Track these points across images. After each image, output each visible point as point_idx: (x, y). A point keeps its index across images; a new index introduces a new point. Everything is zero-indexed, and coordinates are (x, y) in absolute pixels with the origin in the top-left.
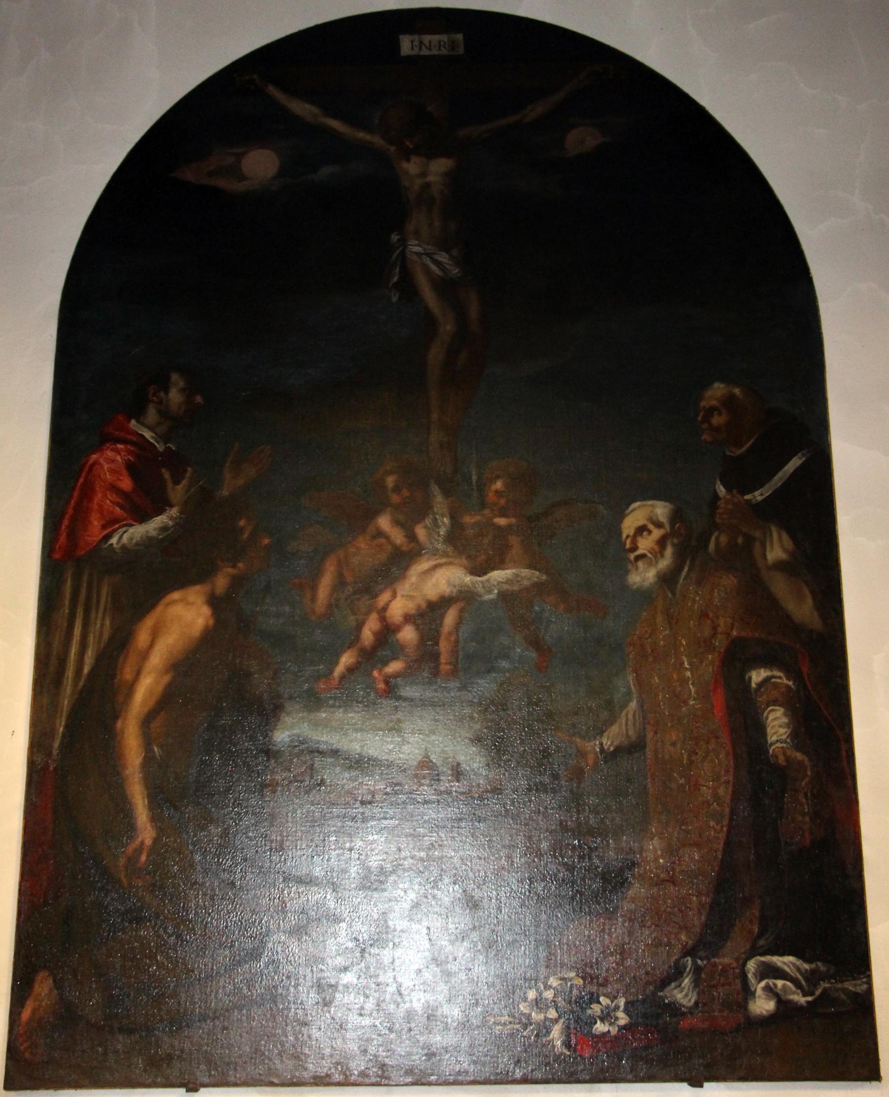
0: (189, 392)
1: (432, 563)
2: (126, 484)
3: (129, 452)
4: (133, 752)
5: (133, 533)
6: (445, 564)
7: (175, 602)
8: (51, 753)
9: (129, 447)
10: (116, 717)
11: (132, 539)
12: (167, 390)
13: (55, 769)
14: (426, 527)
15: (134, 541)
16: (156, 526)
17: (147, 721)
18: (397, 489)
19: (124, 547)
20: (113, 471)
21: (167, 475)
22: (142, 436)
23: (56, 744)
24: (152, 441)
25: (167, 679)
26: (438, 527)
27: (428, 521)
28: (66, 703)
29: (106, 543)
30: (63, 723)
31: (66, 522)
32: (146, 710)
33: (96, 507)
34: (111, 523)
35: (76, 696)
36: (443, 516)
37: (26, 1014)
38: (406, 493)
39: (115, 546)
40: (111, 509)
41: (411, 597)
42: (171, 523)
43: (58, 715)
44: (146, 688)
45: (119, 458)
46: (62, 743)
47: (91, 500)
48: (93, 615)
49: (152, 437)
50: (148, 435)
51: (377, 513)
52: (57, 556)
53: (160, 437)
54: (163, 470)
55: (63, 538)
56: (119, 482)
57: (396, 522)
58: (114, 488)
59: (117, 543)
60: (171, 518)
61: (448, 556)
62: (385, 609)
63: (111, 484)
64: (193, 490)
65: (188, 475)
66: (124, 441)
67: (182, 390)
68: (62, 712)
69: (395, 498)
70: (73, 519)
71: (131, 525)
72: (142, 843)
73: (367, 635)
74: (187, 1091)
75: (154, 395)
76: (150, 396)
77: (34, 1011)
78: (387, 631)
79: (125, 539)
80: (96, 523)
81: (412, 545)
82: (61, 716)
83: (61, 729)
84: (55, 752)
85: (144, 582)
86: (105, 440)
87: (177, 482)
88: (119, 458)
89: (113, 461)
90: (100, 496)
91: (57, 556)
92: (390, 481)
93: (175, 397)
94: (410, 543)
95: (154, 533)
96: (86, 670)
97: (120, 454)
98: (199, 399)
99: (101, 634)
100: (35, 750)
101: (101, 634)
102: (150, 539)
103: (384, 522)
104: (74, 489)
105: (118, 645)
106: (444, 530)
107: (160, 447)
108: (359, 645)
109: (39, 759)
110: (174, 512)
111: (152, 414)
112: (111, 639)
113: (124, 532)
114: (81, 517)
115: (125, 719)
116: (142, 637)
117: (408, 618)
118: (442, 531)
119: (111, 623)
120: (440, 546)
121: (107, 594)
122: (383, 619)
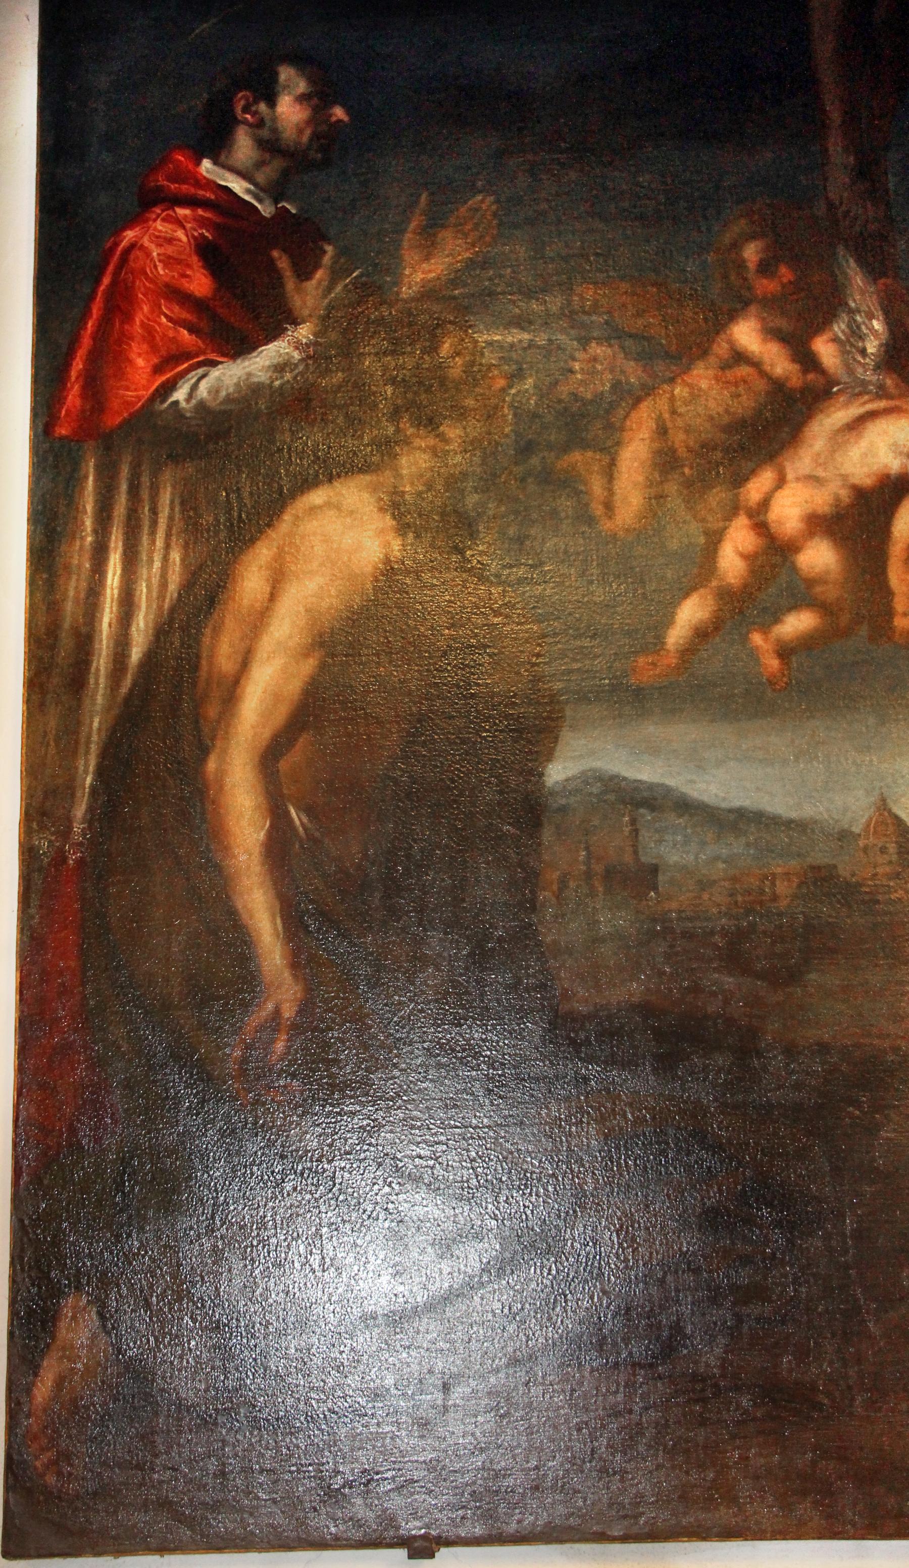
0: (319, 98)
1: (855, 411)
2: (200, 283)
3: (202, 222)
4: (244, 823)
5: (219, 379)
6: (887, 412)
7: (313, 510)
8: (66, 834)
9: (200, 212)
10: (204, 751)
11: (217, 392)
12: (272, 101)
13: (80, 862)
14: (835, 340)
15: (223, 393)
16: (267, 363)
17: (270, 757)
18: (765, 268)
19: (202, 406)
20: (168, 261)
21: (283, 263)
22: (226, 188)
23: (80, 811)
24: (247, 198)
25: (309, 666)
26: (862, 338)
27: (839, 328)
28: (96, 724)
29: (163, 401)
30: (91, 769)
31: (78, 365)
32: (267, 734)
33: (137, 329)
34: (173, 362)
35: (116, 711)
36: (871, 316)
37: (43, 1390)
38: (785, 273)
39: (183, 404)
40: (171, 334)
41: (813, 479)
42: (296, 355)
43: (82, 750)
44: (267, 684)
45: (180, 234)
46: (90, 809)
47: (129, 318)
48: (145, 539)
49: (248, 191)
50: (238, 186)
51: (732, 316)
52: (63, 431)
53: (262, 189)
54: (275, 254)
55: (73, 397)
56: (183, 280)
57: (772, 333)
58: (176, 294)
59: (188, 400)
60: (298, 346)
61: (888, 396)
62: (765, 504)
63: (167, 285)
64: (339, 288)
65: (327, 260)
66: (192, 202)
67: (302, 99)
68: (88, 742)
69: (766, 286)
70: (94, 356)
71: (214, 364)
72: (277, 1012)
73: (733, 557)
74: (410, 1557)
75: (246, 110)
76: (238, 110)
77: (59, 1383)
78: (776, 551)
79: (203, 390)
80: (140, 362)
81: (811, 376)
82: (87, 753)
83: (89, 780)
84: (77, 828)
85: (236, 477)
86: (151, 200)
87: (304, 273)
88: (180, 234)
89: (170, 241)
90: (146, 309)
91: (63, 431)
92: (751, 253)
93: (289, 112)
94: (805, 371)
95: (262, 377)
96: (136, 654)
97: (184, 228)
98: (339, 113)
99: (164, 585)
100: (35, 825)
101: (164, 585)
102: (256, 390)
103: (746, 334)
104: (92, 297)
105: (202, 598)
106: (876, 343)
107: (266, 209)
108: (714, 583)
109: (43, 844)
110: (304, 332)
111: (244, 147)
112: (188, 586)
113: (204, 376)
114: (108, 354)
115: (224, 751)
116: (251, 582)
117: (819, 524)
118: (872, 347)
119: (183, 560)
120: (870, 376)
121: (172, 502)
122: (761, 527)
